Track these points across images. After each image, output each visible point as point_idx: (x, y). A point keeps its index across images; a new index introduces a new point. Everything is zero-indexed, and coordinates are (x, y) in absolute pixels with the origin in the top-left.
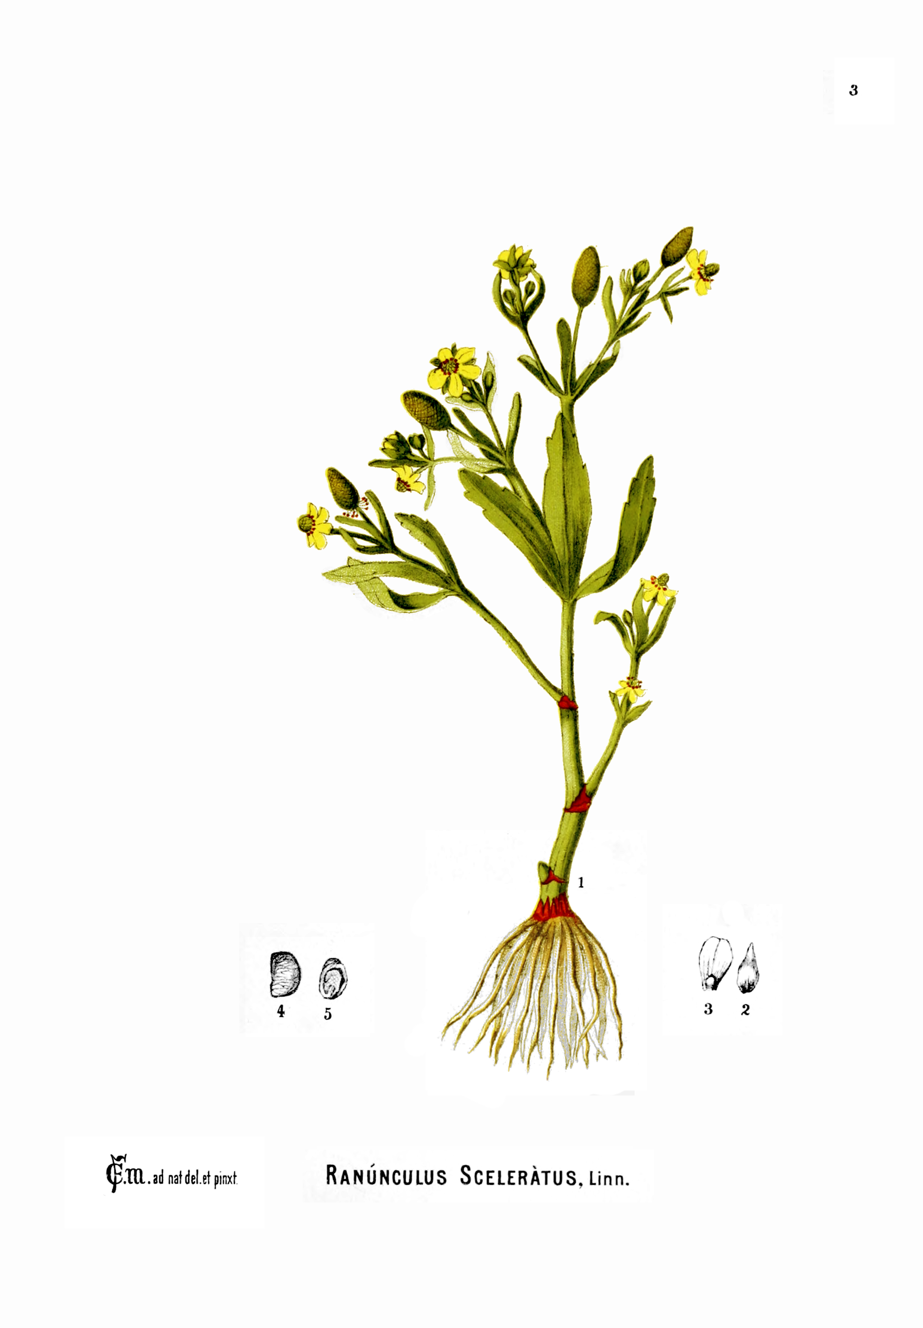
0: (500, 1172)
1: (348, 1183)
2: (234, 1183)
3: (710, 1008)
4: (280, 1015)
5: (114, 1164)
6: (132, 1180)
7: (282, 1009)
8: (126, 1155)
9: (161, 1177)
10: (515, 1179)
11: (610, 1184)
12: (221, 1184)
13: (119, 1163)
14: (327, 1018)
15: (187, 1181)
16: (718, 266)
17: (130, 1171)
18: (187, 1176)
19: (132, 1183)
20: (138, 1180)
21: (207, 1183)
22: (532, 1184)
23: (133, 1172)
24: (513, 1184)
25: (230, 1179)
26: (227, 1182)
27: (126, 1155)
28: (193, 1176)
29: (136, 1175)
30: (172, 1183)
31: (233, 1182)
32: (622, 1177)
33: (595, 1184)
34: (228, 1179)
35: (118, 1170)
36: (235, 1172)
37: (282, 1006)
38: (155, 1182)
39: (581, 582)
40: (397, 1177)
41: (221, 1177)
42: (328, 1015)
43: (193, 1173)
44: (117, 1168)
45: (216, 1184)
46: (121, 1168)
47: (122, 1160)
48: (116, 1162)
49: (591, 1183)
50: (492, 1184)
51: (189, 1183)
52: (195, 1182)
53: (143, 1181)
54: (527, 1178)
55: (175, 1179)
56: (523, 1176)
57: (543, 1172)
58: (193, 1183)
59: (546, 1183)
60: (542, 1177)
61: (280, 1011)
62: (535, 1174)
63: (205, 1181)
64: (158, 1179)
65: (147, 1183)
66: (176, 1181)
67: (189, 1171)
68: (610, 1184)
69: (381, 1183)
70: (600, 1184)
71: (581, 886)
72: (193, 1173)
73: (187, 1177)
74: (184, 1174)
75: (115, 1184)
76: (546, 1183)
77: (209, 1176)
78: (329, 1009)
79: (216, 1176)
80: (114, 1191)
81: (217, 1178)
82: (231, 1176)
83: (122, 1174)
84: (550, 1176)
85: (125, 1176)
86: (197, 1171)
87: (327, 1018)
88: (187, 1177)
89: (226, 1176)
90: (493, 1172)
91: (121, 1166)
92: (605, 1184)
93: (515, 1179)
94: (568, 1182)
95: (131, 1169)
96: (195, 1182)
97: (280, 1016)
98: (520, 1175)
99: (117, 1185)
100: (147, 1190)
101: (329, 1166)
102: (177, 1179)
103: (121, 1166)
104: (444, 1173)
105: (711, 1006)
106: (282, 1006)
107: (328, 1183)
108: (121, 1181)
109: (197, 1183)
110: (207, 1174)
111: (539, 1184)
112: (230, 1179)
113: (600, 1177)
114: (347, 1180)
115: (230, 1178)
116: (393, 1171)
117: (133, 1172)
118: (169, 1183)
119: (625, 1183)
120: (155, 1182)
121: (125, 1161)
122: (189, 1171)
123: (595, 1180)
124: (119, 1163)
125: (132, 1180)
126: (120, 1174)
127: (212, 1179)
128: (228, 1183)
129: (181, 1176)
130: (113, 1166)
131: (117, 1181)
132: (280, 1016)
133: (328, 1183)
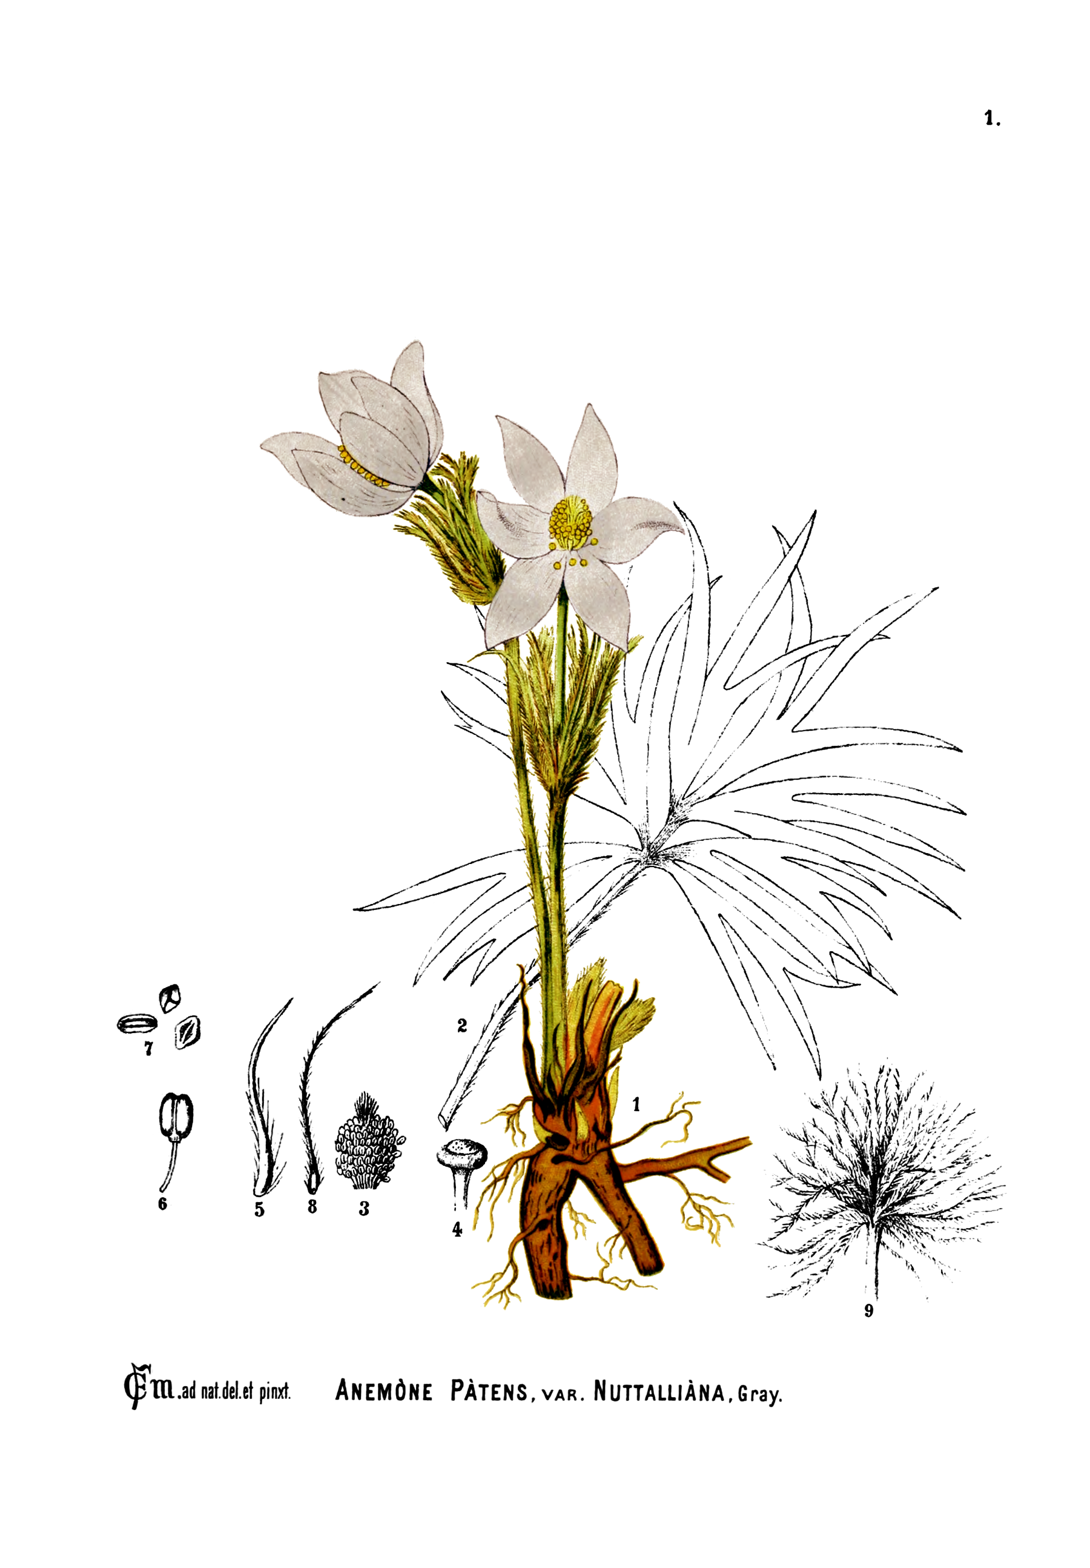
1: (475, 1399)
2: (286, 1397)
3: (365, 1208)
4: (455, 1234)
5: (135, 1374)
6: (159, 1393)
7: (458, 1228)
10: (375, 1394)
12: (268, 1398)
13: (142, 1373)
14: (259, 1214)
15: (225, 1395)
17: (155, 1382)
18: (224, 1388)
19: (159, 1397)
20: (166, 1394)
22: (646, 1399)
23: (159, 1384)
25: (281, 1392)
26: (278, 1396)
28: (232, 1388)
29: (164, 1389)
33: (664, 1399)
34: (278, 1393)
37: (458, 1224)
41: (268, 1389)
42: (259, 1210)
44: (140, 1378)
46: (145, 1381)
47: (146, 1371)
48: (137, 1371)
51: (618, 1399)
52: (247, 1396)
55: (210, 1393)
56: (508, 1391)
58: (232, 1398)
60: (479, 1392)
61: (456, 1229)
63: (246, 1394)
64: (189, 1393)
65: (176, 1397)
66: (185, 1395)
67: (227, 1382)
69: (411, 1399)
71: (637, 1109)
72: (232, 1384)
73: (225, 1390)
74: (221, 1386)
75: (136, 1399)
77: (251, 1387)
80: (135, 1407)
85: (150, 1388)
86: (237, 1382)
87: (259, 1214)
88: (225, 1390)
89: (276, 1388)
91: (144, 1377)
92: (484, 1399)
94: (518, 1395)
95: (164, 1380)
97: (456, 1236)
99: (139, 1401)
101: (454, 1381)
102: (212, 1392)
103: (144, 1377)
104: (525, 1388)
106: (458, 1224)
107: (596, 1399)
109: (237, 1398)
110: (248, 1386)
111: (654, 1399)
112: (281, 1392)
114: (693, 1395)
117: (159, 1384)
118: (203, 1397)
122: (227, 1382)
124: (142, 1373)
125: (159, 1393)
126: (143, 1387)
127: (256, 1393)
128: (279, 1398)
129: (217, 1388)
130: (133, 1376)
131: (140, 1396)
132: (456, 1236)
133: (596, 1399)
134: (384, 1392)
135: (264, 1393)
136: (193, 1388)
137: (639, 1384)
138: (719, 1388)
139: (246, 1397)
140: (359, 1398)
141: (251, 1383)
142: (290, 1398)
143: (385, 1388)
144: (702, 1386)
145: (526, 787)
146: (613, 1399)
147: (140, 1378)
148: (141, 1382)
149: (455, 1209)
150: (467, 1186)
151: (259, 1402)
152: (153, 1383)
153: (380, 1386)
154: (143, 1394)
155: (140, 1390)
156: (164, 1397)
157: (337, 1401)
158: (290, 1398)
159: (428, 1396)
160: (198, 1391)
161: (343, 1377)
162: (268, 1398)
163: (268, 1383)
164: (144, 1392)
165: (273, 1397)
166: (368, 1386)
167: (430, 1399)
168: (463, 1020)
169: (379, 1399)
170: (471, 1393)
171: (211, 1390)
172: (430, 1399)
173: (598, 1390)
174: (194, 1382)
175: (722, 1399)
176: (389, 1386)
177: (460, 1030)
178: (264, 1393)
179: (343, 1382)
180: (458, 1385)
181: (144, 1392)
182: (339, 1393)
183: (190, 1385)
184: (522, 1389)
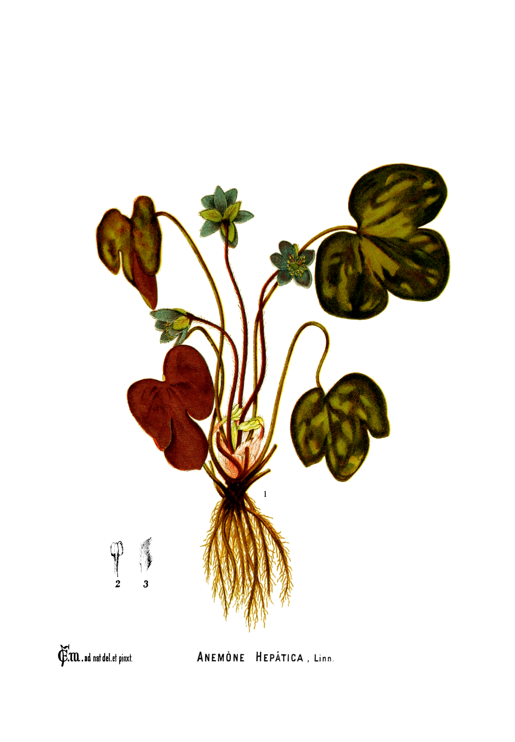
0: (288, 655)
2: (130, 661)
5: (62, 650)
6: (73, 659)
8: (69, 645)
9: (89, 658)
10: (268, 658)
11: (260, 660)
12: (123, 661)
13: (65, 650)
15: (104, 660)
16: (345, 478)
17: (71, 654)
19: (73, 661)
21: (115, 660)
23: (73, 655)
24: (267, 661)
25: (127, 659)
26: (126, 660)
27: (69, 645)
28: (107, 657)
29: (75, 657)
30: (95, 661)
32: (330, 658)
33: (318, 661)
34: (127, 659)
35: (65, 653)
36: (130, 655)
38: (86, 660)
39: (208, 440)
40: (294, 658)
41: (123, 657)
43: (107, 655)
44: (64, 652)
45: (120, 661)
46: (67, 653)
47: (67, 648)
48: (63, 649)
49: (315, 661)
50: (267, 661)
52: (114, 660)
53: (79, 660)
57: (282, 655)
58: (107, 661)
59: (284, 660)
60: (281, 658)
63: (114, 660)
64: (88, 659)
65: (81, 661)
66: (98, 660)
67: (105, 654)
68: (260, 660)
70: (320, 661)
72: (107, 655)
73: (104, 658)
74: (102, 655)
75: (63, 661)
76: (284, 660)
77: (116, 657)
79: (120, 657)
80: (62, 665)
81: (120, 658)
82: (129, 657)
83: (67, 656)
84: (286, 657)
85: (69, 657)
86: (109, 654)
88: (104, 658)
89: (125, 657)
91: (66, 651)
93: (268, 658)
95: (72, 653)
96: (108, 660)
98: (271, 656)
100: (81, 665)
102: (98, 659)
103: (66, 651)
108: (66, 660)
109: (109, 661)
110: (115, 656)
111: (202, 661)
112: (127, 659)
113: (320, 658)
114: (201, 659)
115: (128, 658)
116: (226, 655)
117: (73, 655)
118: (94, 661)
120: (86, 660)
121: (69, 649)
122: (105, 654)
123: (317, 659)
124: (65, 650)
125: (73, 659)
126: (66, 656)
128: (127, 661)
129: (100, 657)
131: (65, 660)
133: (257, 660)
134: (221, 658)
135: (121, 659)
136: (89, 657)
137: (284, 654)
138: (300, 655)
140: (209, 660)
141: (100, 654)
142: (132, 661)
143: (221, 656)
144: (206, 655)
145: (124, 265)
146: (227, 660)
147: (64, 652)
148: (65, 653)
150: (291, 569)
152: (70, 654)
153: (219, 655)
154: (66, 659)
156: (75, 661)
157: (198, 662)
158: (132, 661)
159: (242, 659)
161: (219, 653)
162: (123, 661)
163: (122, 654)
164: (66, 658)
165: (124, 661)
167: (243, 661)
169: (219, 661)
170: (278, 659)
171: (98, 658)
172: (243, 661)
173: (219, 657)
174: (90, 654)
175: (280, 661)
176: (223, 655)
178: (121, 659)
179: (200, 653)
180: (272, 656)
182: (199, 659)
183: (88, 655)
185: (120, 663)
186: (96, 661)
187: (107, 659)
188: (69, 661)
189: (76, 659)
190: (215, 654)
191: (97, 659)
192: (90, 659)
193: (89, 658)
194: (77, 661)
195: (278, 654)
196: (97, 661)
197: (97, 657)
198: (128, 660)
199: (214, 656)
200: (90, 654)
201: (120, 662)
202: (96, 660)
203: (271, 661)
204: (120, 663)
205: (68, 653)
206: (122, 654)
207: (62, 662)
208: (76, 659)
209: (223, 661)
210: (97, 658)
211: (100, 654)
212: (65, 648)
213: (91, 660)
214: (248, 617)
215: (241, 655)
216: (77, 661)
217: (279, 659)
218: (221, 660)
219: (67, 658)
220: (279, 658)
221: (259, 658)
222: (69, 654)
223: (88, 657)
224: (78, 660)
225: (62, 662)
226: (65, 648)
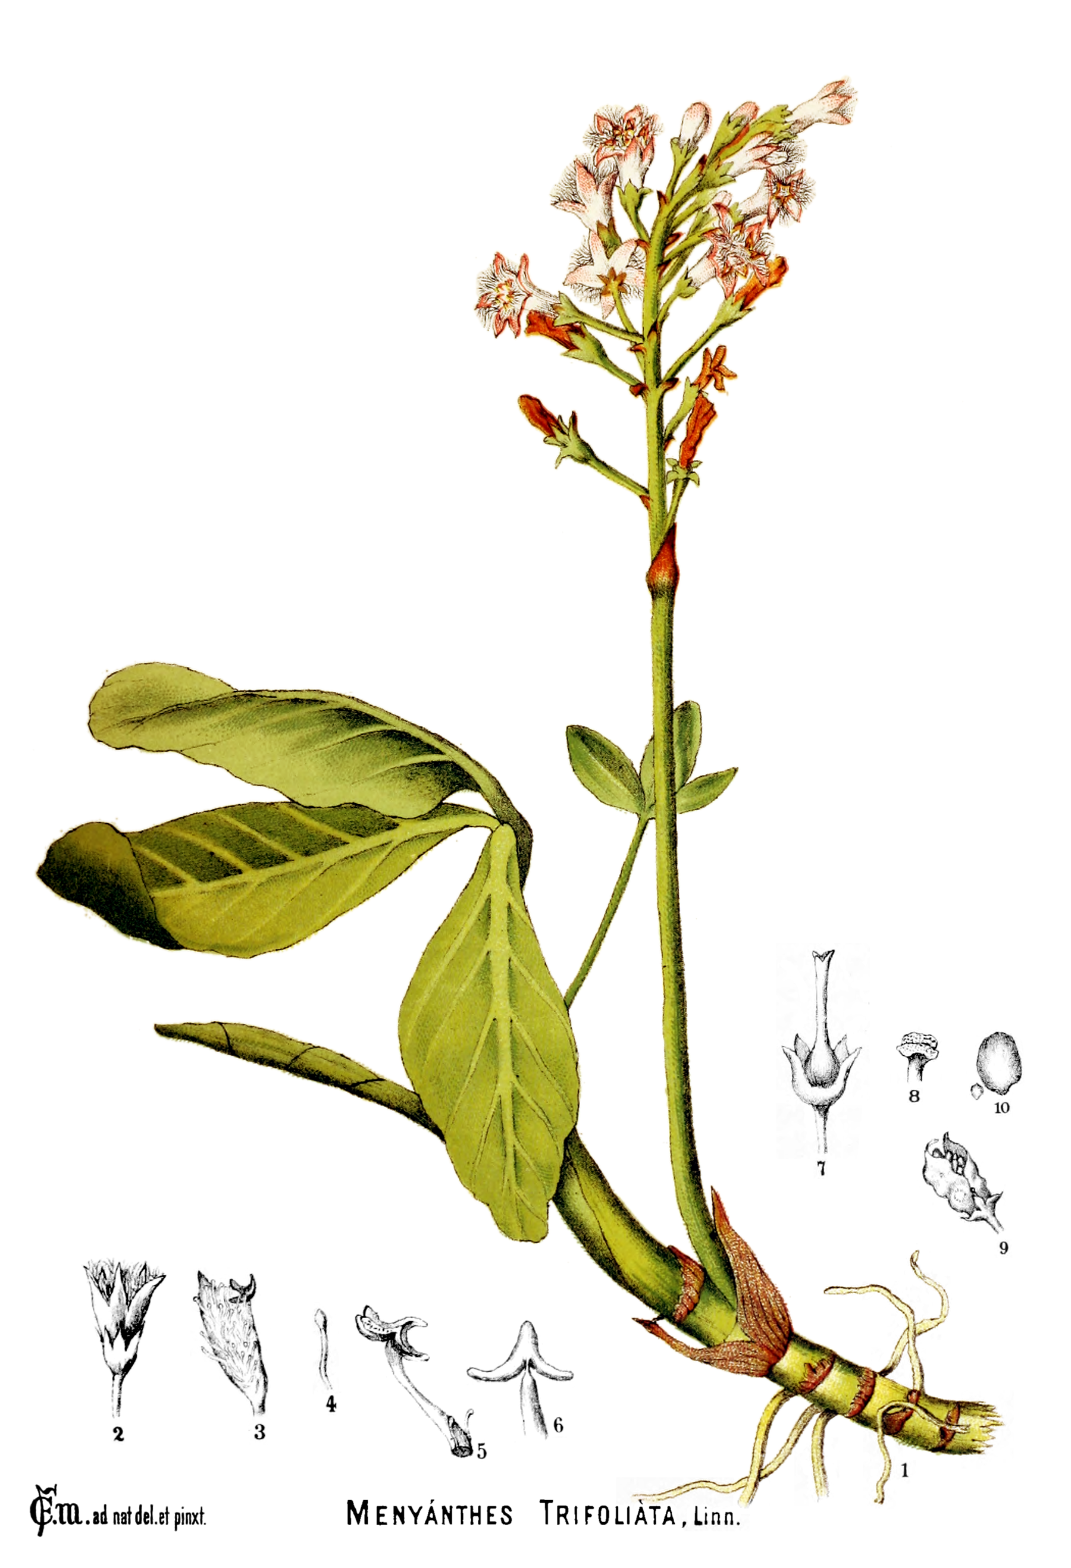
2: (201, 1523)
4: (329, 1409)
5: (40, 1498)
6: (65, 1519)
8: (56, 1486)
11: (479, 1523)
12: (183, 1524)
13: (48, 1496)
17: (61, 1506)
19: (65, 1523)
23: (65, 1508)
24: (494, 1523)
25: (194, 1518)
26: (192, 1521)
27: (56, 1486)
28: (146, 1513)
29: (70, 1514)
30: (119, 1523)
31: (199, 1521)
32: (731, 1514)
33: (622, 1523)
34: (193, 1518)
35: (46, 1505)
36: (202, 1508)
37: (332, 1398)
38: (96, 1522)
41: (183, 1514)
42: (482, 1453)
45: (177, 1523)
46: (51, 1505)
47: (52, 1493)
48: (43, 1495)
50: (494, 1523)
52: (163, 1522)
54: (567, 1516)
55: (123, 1518)
57: (651, 1508)
58: (146, 1523)
60: (649, 1514)
61: (330, 1403)
62: (641, 1510)
63: (162, 1520)
64: (99, 1518)
67: (141, 1506)
71: (905, 1475)
72: (146, 1509)
74: (135, 1510)
75: (42, 1524)
77: (167, 1513)
78: (483, 1444)
80: (40, 1534)
81: (178, 1516)
82: (197, 1514)
83: (52, 1511)
85: (56, 1513)
86: (152, 1506)
89: (189, 1514)
90: (385, 1508)
91: (50, 1500)
94: (502, 1520)
102: (125, 1518)
103: (50, 1500)
104: (510, 1510)
105: (263, 1428)
106: (332, 1398)
109: (152, 1523)
110: (126, 1511)
112: (194, 1518)
114: (434, 1519)
115: (195, 1517)
117: (65, 1508)
119: (735, 1523)
120: (96, 1522)
121: (55, 1494)
122: (141, 1506)
124: (48, 1496)
125: (65, 1519)
126: (49, 1511)
127: (172, 1518)
128: (193, 1523)
129: (130, 1513)
131: (46, 1521)
133: (349, 1522)
136: (104, 1513)
137: (462, 1505)
139: (162, 1523)
141: (129, 1508)
144: (444, 1508)
148: (46, 1505)
149: (261, 1432)
151: (174, 1529)
152: (58, 1507)
155: (46, 1514)
156: (70, 1522)
160: (110, 1517)
162: (183, 1524)
163: (183, 1508)
164: (50, 1515)
165: (187, 1523)
166: (588, 1508)
168: (120, 1429)
170: (431, 1518)
173: (352, 1512)
174: (105, 1506)
177: (118, 1438)
181: (50, 1515)
183: (100, 1510)
184: (506, 1510)
185: (176, 1529)
186: (121, 1524)
187: (147, 1520)
188: (55, 1522)
189: (73, 1519)
190: (385, 1508)
191: (122, 1519)
192: (106, 1519)
193: (103, 1516)
194: (75, 1524)
195: (432, 1505)
196: (123, 1523)
197: (123, 1513)
198: (195, 1520)
199: (492, 1511)
200: (105, 1506)
201: (178, 1526)
202: (120, 1521)
203: (636, 1523)
204: (176, 1529)
205: (54, 1503)
206: (183, 1508)
207: (39, 1526)
208: (73, 1519)
209: (366, 1522)
210: (122, 1515)
211: (129, 1508)
212: (45, 1493)
213: (108, 1521)
214: (906, 1332)
215: (489, 1508)
216: (75, 1524)
217: (644, 1519)
218: (358, 1521)
219: (51, 1517)
220: (644, 1515)
221: (476, 1519)
222: (56, 1507)
223: (102, 1514)
224: (77, 1521)
225: (39, 1526)
226: (45, 1493)
